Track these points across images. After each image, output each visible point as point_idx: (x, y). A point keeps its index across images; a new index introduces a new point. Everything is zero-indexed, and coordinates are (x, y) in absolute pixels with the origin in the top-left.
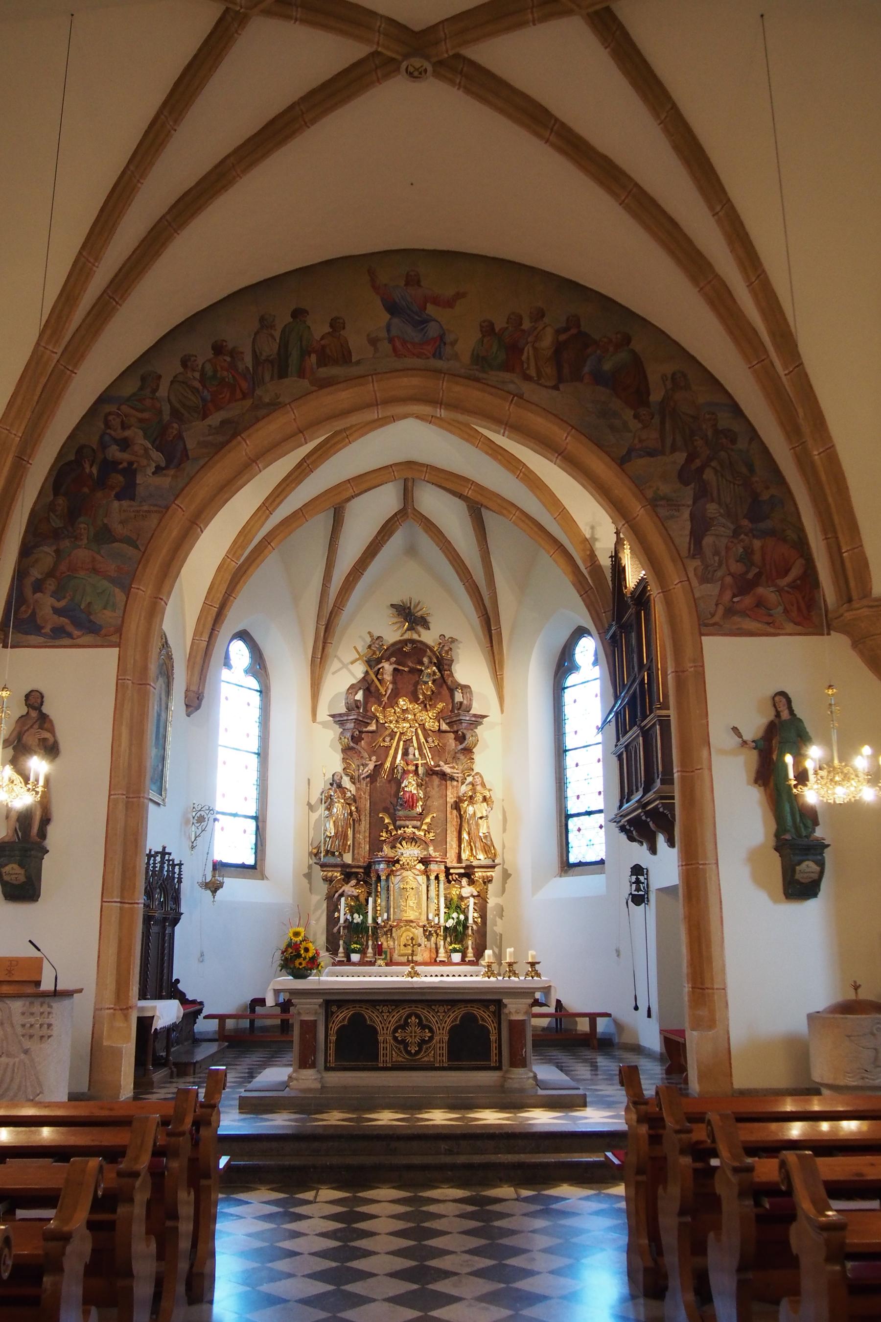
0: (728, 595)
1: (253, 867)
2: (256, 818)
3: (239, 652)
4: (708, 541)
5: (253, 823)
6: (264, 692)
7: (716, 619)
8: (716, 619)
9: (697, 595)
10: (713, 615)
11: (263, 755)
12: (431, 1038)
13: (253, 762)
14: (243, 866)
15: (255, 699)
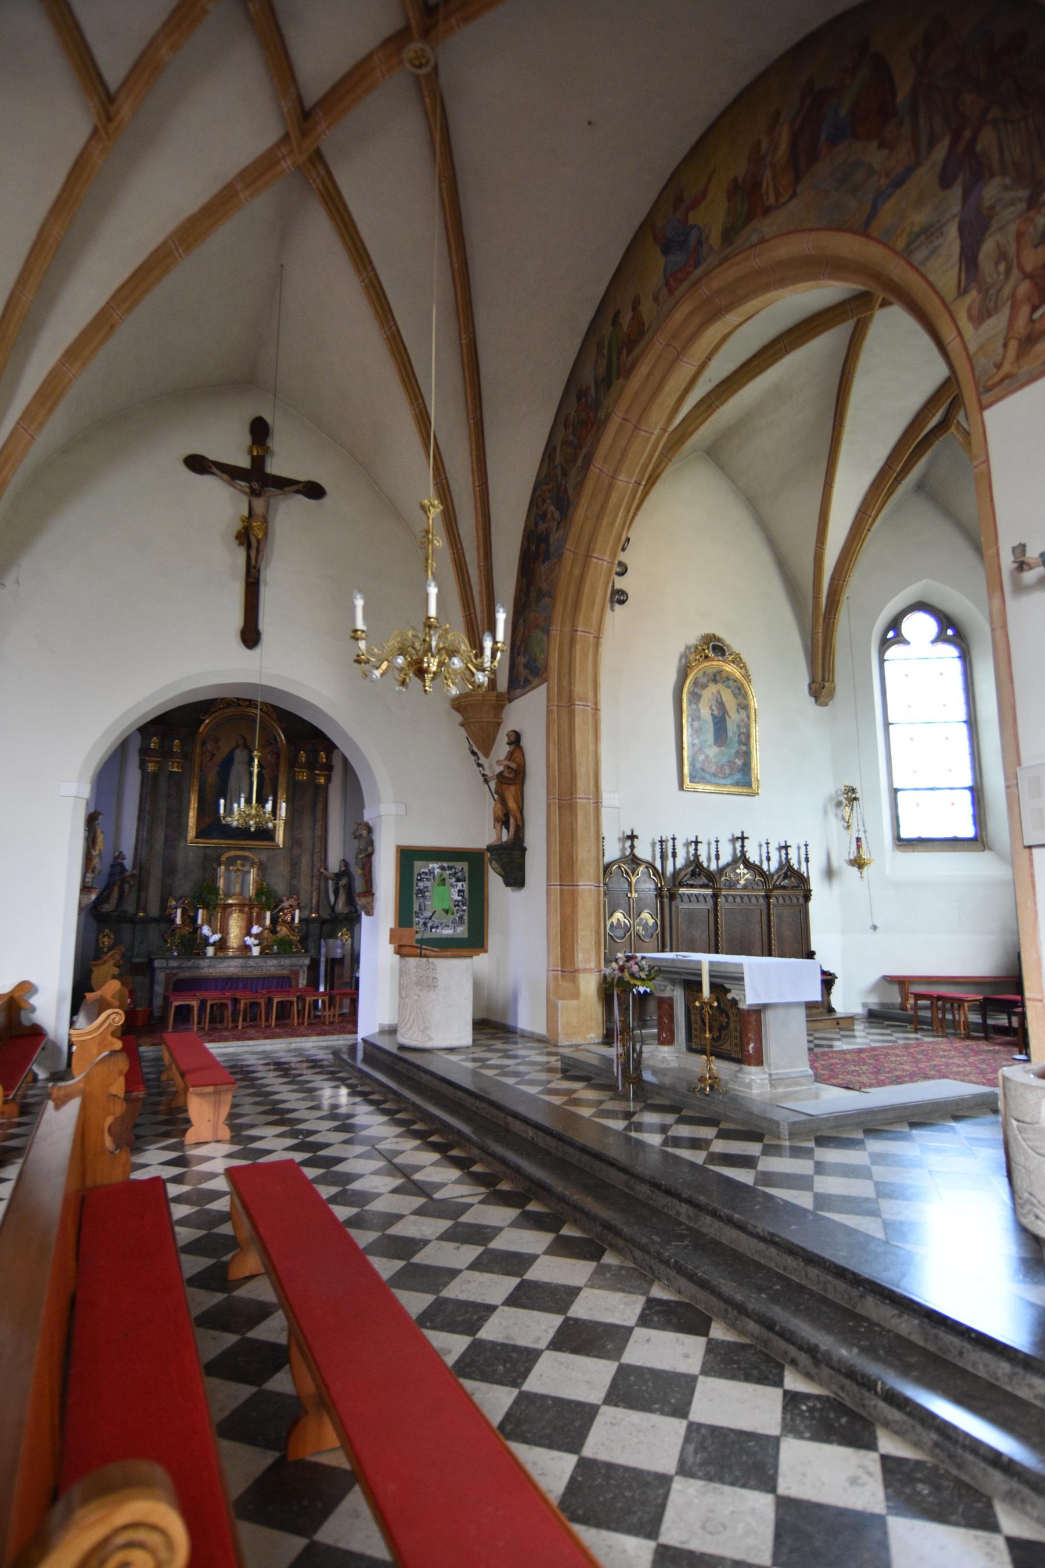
0: (1025, 311)
1: (974, 839)
2: (971, 789)
3: (920, 627)
4: (988, 246)
5: (968, 794)
6: (965, 657)
7: (1006, 368)
8: (1006, 368)
9: (972, 348)
10: (998, 366)
11: (972, 723)
12: (728, 1023)
13: (964, 729)
14: (955, 840)
15: (957, 666)
